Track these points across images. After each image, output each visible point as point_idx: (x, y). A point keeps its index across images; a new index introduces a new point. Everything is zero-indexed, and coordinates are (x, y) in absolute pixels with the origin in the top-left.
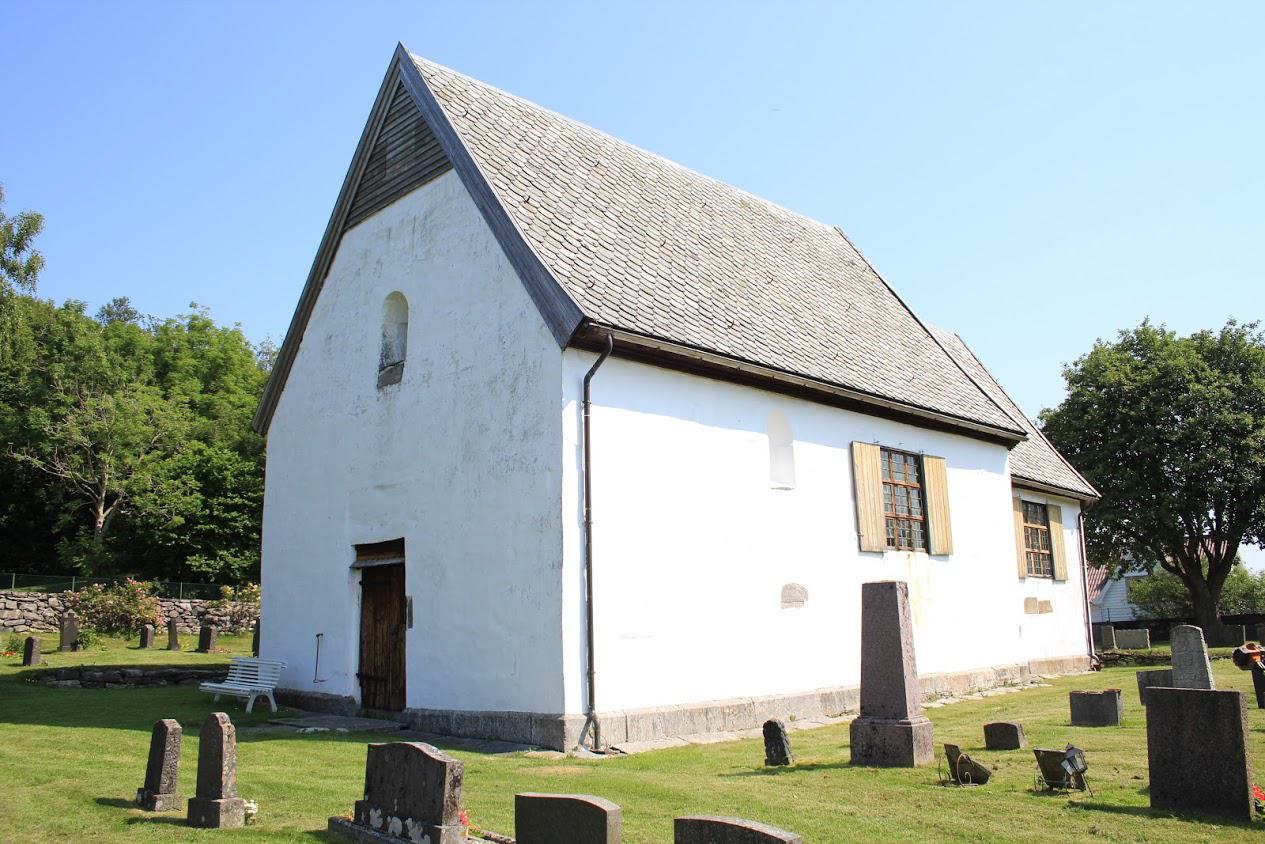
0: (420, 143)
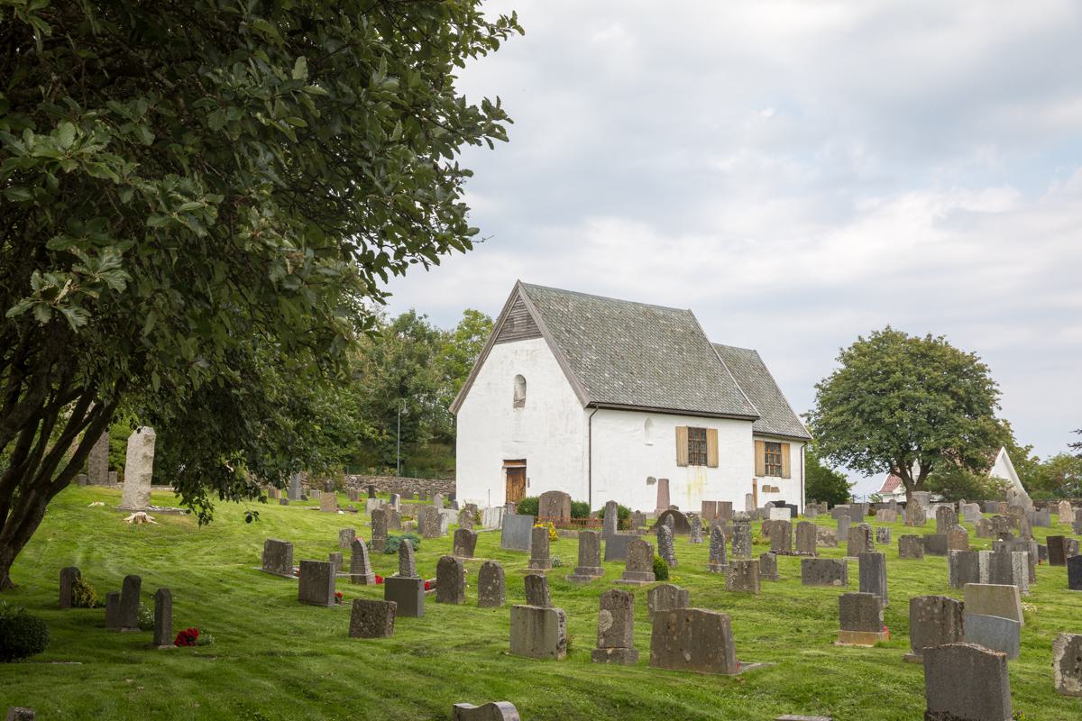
0: (529, 323)
